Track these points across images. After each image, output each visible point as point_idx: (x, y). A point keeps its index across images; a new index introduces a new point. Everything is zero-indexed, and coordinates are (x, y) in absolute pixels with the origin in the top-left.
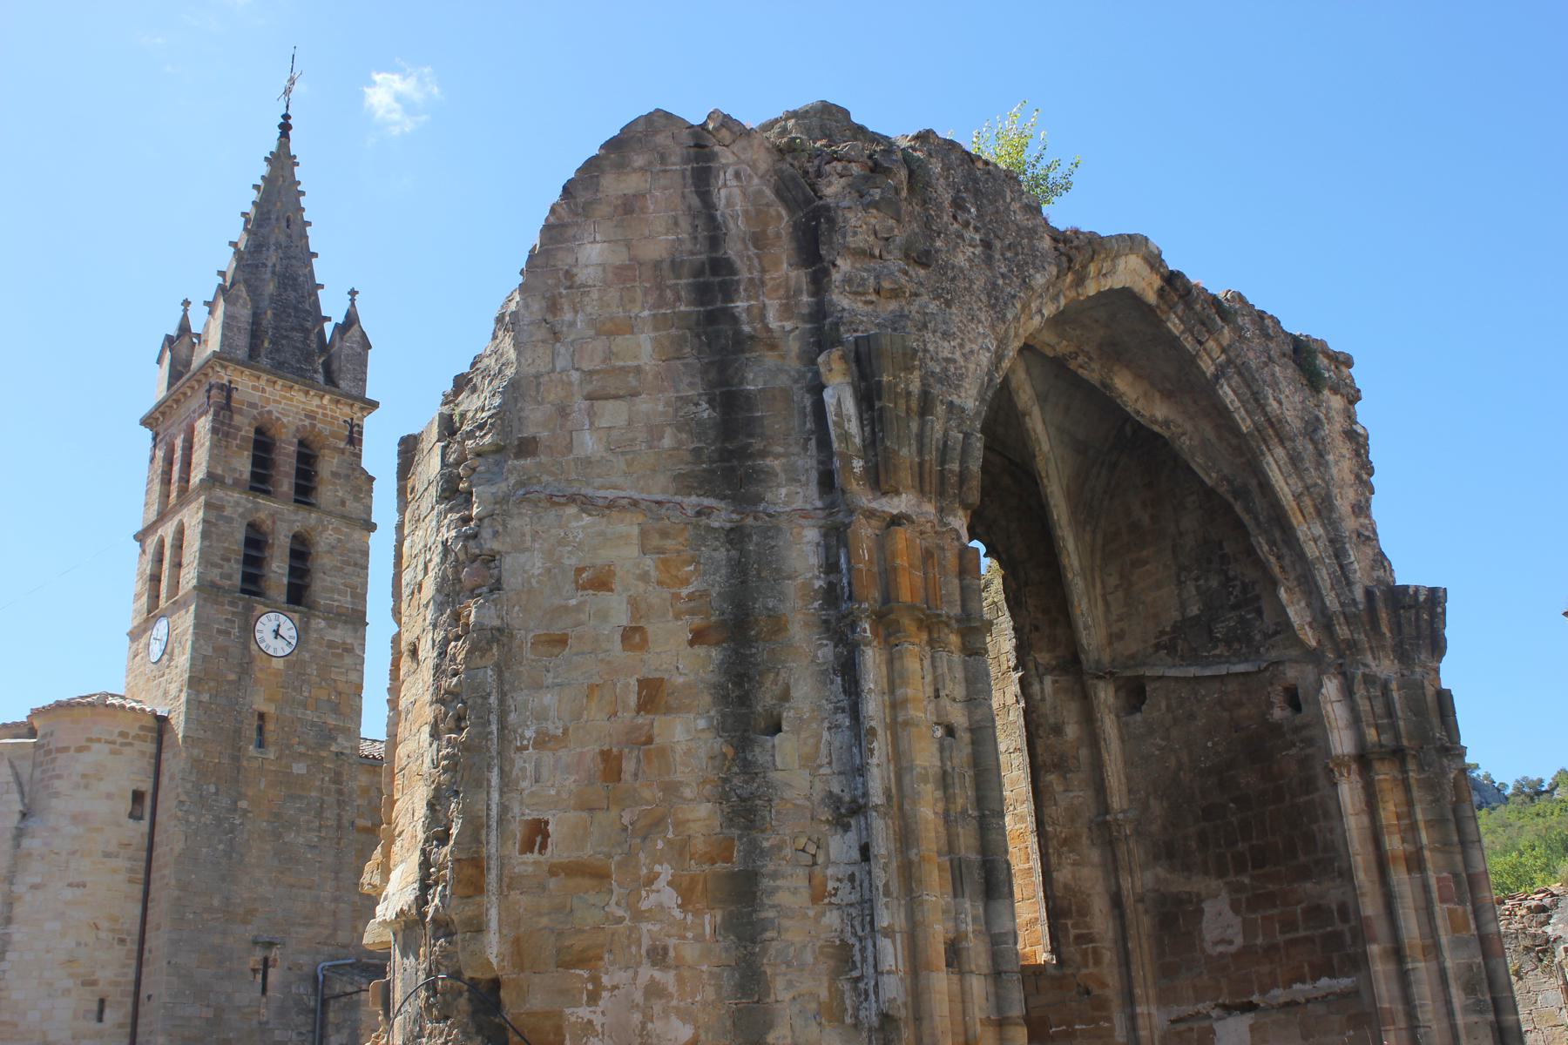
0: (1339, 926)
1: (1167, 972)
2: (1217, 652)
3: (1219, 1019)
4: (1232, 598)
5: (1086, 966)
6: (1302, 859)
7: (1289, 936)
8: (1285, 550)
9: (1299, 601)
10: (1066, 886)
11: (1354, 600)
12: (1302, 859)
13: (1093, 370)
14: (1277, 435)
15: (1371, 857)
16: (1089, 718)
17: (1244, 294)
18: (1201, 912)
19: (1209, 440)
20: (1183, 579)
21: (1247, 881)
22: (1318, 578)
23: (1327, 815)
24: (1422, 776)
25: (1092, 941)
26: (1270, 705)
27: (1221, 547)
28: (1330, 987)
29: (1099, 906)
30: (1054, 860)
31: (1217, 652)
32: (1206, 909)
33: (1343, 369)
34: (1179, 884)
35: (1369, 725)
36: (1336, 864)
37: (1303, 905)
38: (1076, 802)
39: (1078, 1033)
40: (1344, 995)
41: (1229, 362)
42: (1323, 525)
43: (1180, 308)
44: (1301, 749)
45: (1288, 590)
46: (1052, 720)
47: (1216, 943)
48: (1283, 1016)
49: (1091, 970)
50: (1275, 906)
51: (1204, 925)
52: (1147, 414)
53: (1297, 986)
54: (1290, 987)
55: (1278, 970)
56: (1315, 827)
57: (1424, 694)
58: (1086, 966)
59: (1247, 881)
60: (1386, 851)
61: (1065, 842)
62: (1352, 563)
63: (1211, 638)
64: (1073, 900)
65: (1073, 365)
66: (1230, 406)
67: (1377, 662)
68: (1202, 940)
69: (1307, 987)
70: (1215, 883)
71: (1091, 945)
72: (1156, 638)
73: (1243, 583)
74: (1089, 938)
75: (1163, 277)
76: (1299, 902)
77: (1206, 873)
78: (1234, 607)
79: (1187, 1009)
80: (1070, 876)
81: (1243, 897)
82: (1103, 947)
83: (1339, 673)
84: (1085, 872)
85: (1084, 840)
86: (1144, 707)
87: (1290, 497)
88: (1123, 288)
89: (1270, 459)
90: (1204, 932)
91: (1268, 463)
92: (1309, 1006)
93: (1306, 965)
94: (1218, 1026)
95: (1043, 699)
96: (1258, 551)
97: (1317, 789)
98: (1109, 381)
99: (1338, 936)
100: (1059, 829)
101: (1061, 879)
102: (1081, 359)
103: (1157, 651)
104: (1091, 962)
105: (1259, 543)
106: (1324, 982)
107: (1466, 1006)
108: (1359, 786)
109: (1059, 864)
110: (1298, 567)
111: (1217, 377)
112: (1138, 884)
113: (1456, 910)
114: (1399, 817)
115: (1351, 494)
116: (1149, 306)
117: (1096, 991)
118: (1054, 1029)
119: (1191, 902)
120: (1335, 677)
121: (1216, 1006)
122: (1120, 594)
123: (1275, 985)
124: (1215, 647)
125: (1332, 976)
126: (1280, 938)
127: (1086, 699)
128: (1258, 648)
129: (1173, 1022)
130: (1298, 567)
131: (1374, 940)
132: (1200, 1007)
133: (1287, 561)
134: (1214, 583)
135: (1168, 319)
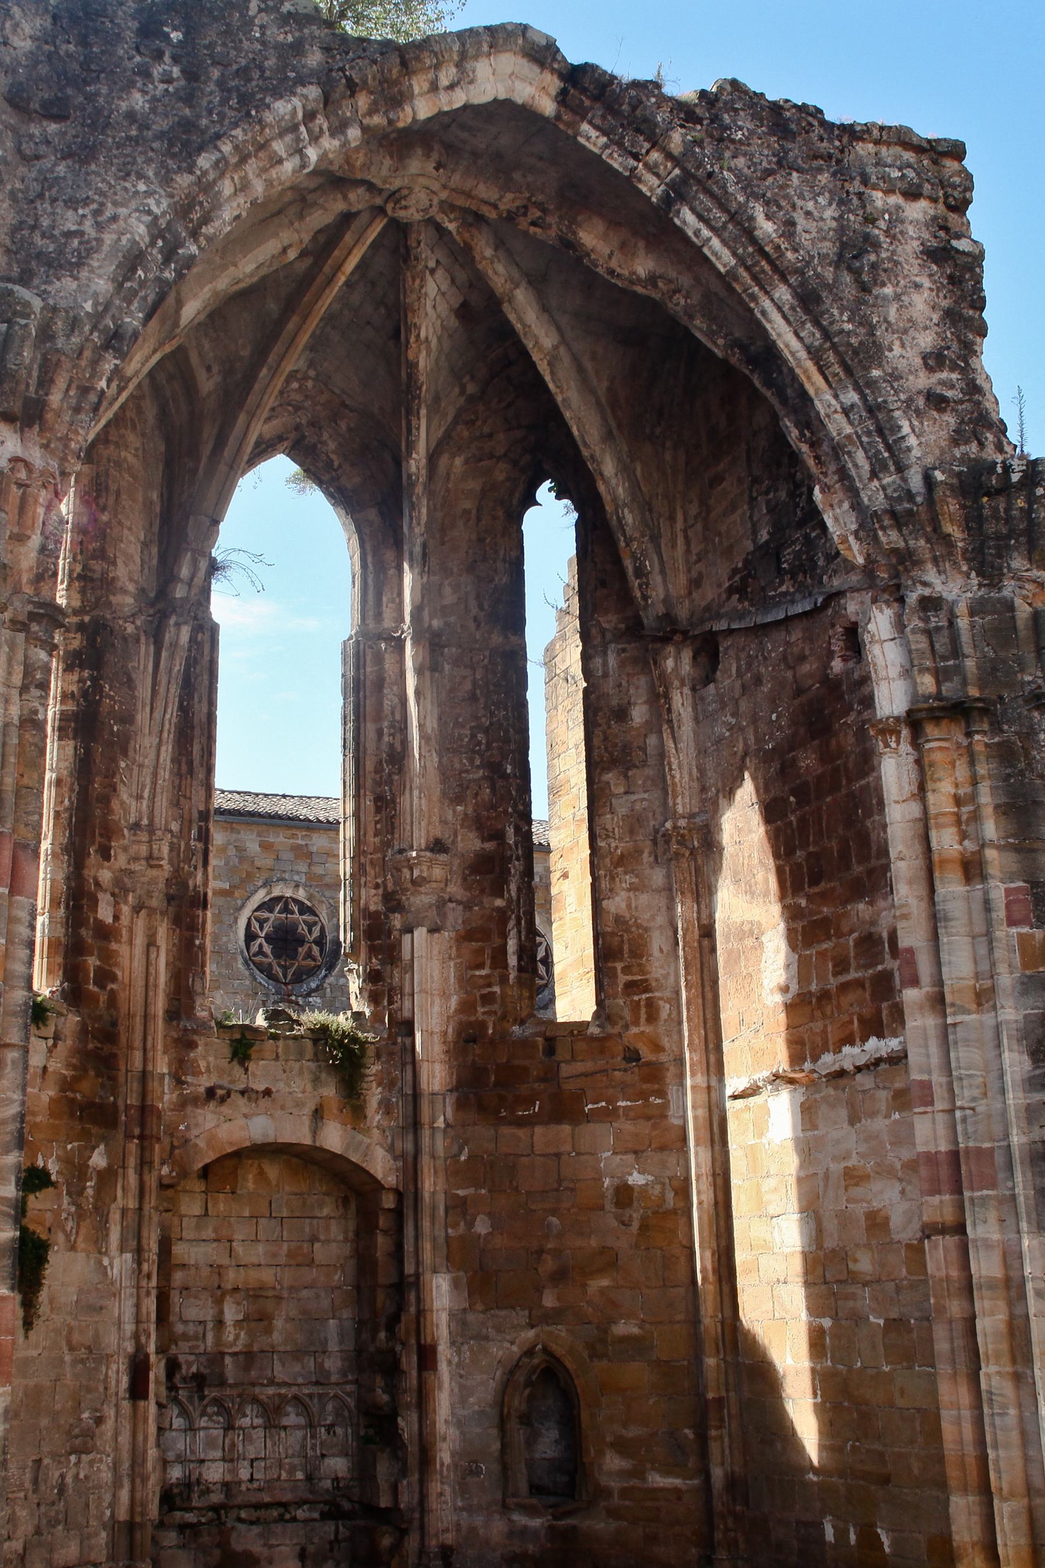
2: (784, 588)
6: (858, 869)
7: (842, 979)
9: (841, 502)
11: (909, 491)
12: (858, 869)
13: (550, 226)
14: (775, 268)
15: (919, 863)
16: (659, 700)
17: (741, 79)
19: (716, 294)
20: (755, 495)
21: (803, 903)
22: (850, 465)
24: (996, 740)
25: (647, 990)
30: (604, 884)
31: (784, 588)
37: (855, 935)
38: (638, 807)
39: (621, 1112)
41: (687, 174)
42: (858, 389)
43: (598, 112)
45: (826, 489)
46: (614, 702)
49: (642, 1029)
53: (847, 1049)
54: (840, 1051)
55: (829, 1029)
57: (1013, 618)
58: (637, 1023)
59: (803, 903)
62: (903, 437)
63: (780, 571)
64: (626, 936)
66: (695, 239)
67: (943, 577)
69: (856, 1050)
71: (644, 996)
72: (729, 579)
75: (562, 76)
76: (851, 932)
80: (623, 905)
82: (661, 998)
84: (644, 899)
85: (646, 858)
87: (803, 354)
88: (495, 100)
89: (767, 304)
91: (764, 313)
92: (858, 1077)
95: (606, 675)
100: (613, 845)
101: (613, 910)
102: (535, 213)
103: (729, 598)
104: (643, 1016)
106: (873, 1042)
107: (1034, 1077)
109: (611, 890)
111: (667, 201)
113: (1032, 936)
114: (958, 801)
116: (546, 120)
117: (647, 1055)
118: (590, 1106)
120: (889, 606)
122: (699, 526)
123: (825, 1049)
125: (880, 1036)
134: (783, 495)
135: (578, 133)
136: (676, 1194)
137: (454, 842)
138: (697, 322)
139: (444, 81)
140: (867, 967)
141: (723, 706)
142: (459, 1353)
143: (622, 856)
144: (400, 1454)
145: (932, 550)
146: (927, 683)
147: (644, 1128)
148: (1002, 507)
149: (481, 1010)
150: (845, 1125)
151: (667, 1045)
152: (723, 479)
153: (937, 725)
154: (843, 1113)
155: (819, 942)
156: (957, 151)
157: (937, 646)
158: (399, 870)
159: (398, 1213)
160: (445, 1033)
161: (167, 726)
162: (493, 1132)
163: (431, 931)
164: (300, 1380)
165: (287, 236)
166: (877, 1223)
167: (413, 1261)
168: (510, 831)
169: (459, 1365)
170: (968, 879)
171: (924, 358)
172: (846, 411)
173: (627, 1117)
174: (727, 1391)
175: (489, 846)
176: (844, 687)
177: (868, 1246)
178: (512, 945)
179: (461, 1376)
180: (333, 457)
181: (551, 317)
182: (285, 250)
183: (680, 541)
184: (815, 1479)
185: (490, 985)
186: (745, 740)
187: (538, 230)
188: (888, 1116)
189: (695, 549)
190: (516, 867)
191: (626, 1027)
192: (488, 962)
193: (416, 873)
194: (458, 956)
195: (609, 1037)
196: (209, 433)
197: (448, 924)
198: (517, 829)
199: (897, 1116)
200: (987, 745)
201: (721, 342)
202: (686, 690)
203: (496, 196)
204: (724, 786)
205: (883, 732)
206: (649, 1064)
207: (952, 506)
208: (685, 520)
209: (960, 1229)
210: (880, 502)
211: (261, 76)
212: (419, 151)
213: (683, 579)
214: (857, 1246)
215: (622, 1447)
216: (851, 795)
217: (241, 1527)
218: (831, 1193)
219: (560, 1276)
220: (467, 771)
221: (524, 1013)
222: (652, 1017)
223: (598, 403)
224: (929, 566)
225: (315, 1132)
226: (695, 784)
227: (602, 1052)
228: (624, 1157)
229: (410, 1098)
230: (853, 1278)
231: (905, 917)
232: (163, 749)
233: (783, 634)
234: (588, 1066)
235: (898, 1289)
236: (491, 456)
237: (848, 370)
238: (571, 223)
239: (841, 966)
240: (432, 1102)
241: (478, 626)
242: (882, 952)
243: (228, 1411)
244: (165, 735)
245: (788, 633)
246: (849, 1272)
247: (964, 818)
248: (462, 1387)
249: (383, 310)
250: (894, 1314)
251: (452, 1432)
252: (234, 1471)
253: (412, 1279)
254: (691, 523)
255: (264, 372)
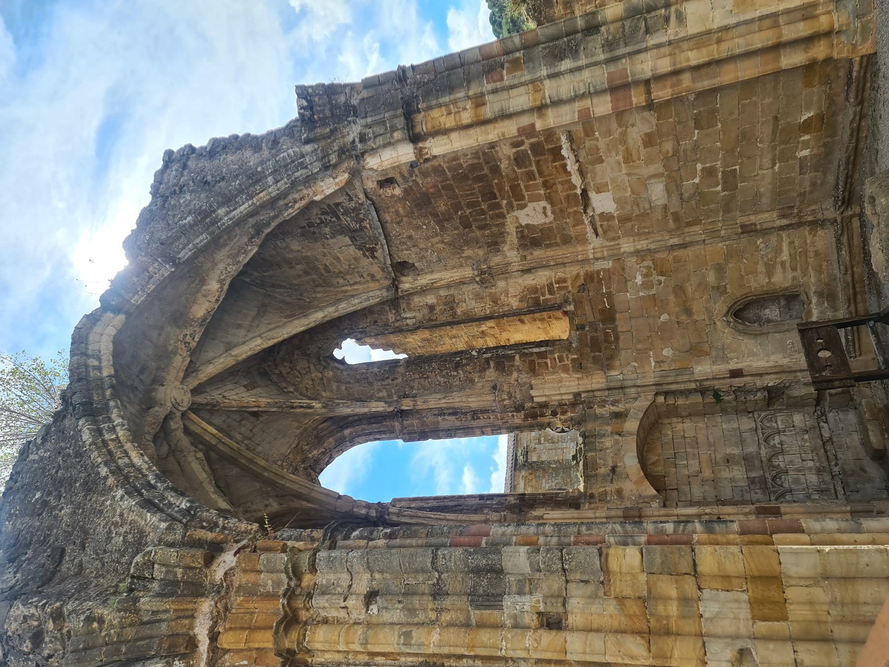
0: (526, 147)
1: (567, 240)
2: (368, 226)
3: (593, 210)
4: (332, 220)
5: (567, 287)
6: (486, 171)
7: (537, 175)
8: (290, 198)
10: (521, 301)
11: (313, 152)
12: (486, 171)
15: (478, 130)
16: (423, 291)
18: (527, 226)
21: (505, 202)
23: (455, 158)
25: (551, 284)
26: (393, 196)
27: (304, 227)
28: (567, 149)
29: (530, 280)
31: (368, 226)
32: (526, 223)
33: (174, 157)
34: (512, 238)
35: (392, 137)
36: (486, 151)
37: (516, 169)
38: (471, 297)
40: (571, 139)
44: (416, 176)
45: (315, 194)
47: (546, 215)
48: (589, 176)
50: (519, 185)
51: (535, 223)
52: (217, 294)
53: (569, 168)
55: (560, 180)
56: (465, 165)
58: (567, 287)
60: (473, 121)
61: (495, 302)
65: (193, 344)
68: (545, 223)
69: (569, 162)
70: (509, 219)
71: (555, 285)
73: (322, 214)
74: (550, 285)
76: (515, 171)
77: (503, 224)
78: (339, 219)
79: (589, 229)
80: (515, 299)
81: (515, 203)
83: (363, 157)
84: (511, 290)
86: (410, 262)
90: (540, 223)
92: (581, 160)
93: (555, 164)
94: (598, 212)
95: (414, 318)
96: (294, 214)
97: (440, 165)
98: (200, 321)
99: (533, 146)
103: (376, 258)
104: (500, 603)
105: (288, 215)
106: (564, 152)
108: (432, 141)
109: (508, 305)
110: (300, 188)
112: (515, 259)
115: (248, 153)
117: (581, 281)
119: (522, 232)
121: (585, 212)
122: (348, 277)
123: (569, 181)
124: (366, 227)
125: (560, 148)
126: (539, 181)
127: (410, 295)
128: (360, 204)
129: (597, 235)
130: (300, 188)
131: (533, 126)
132: (586, 222)
133: (296, 196)
134: (327, 230)
136: (644, 260)
137: (491, 381)
138: (241, 259)
139: (96, 363)
140: (530, 160)
141: (423, 257)
142: (732, 359)
143: (493, 302)
144: (787, 384)
145: (338, 138)
146: (397, 135)
147: (615, 278)
148: (318, 108)
149: (566, 362)
150: (605, 164)
151: (577, 272)
152: (325, 265)
153: (415, 126)
154: (598, 167)
155: (521, 190)
156: (169, 154)
157: (381, 132)
158: (505, 406)
159: (666, 394)
160: (578, 379)
161: (437, 516)
162: (623, 352)
163: (532, 389)
164: (756, 438)
165: (191, 458)
166: (649, 140)
167: (689, 384)
168: (485, 356)
169: (738, 358)
170: (484, 104)
171: (255, 152)
172: (277, 182)
173: (610, 288)
174: (737, 224)
175: (492, 364)
176: (406, 186)
177: (660, 144)
178: (536, 350)
179: (743, 357)
180: (320, 451)
181: (248, 341)
182: (197, 459)
183: (355, 287)
184: (778, 165)
185: (555, 359)
186: (437, 243)
187: (197, 336)
188: (597, 139)
189: (358, 279)
190: (501, 352)
191: (569, 292)
192: (544, 360)
193: (506, 397)
194: (543, 375)
195: (574, 300)
196: (297, 504)
197: (528, 381)
198: (484, 353)
199: (597, 133)
200: (423, 102)
201: (249, 248)
202: (419, 278)
203: (180, 357)
204: (459, 253)
205: (421, 155)
206: (585, 280)
207: (318, 131)
208: (346, 285)
209: (647, 82)
210: (318, 164)
211: (69, 448)
212: (153, 394)
213: (372, 285)
214: (660, 152)
215: (770, 273)
216: (454, 177)
217: (840, 462)
218: (637, 171)
219: (688, 312)
220: (460, 378)
221: (567, 343)
222: (564, 280)
223: (291, 321)
224: (346, 140)
225: (631, 434)
226: (460, 270)
227: (581, 302)
228: (629, 287)
229: (610, 392)
230: (676, 152)
231: (503, 135)
232: (448, 517)
233: (388, 224)
234: (587, 308)
235: (680, 123)
236: (322, 379)
237: (258, 181)
238: (194, 321)
239: (530, 176)
240: (611, 382)
241: (396, 379)
242: (522, 151)
243: (778, 473)
244: (441, 517)
245: (386, 222)
246: (673, 156)
247: (456, 110)
248: (749, 356)
249: (243, 422)
250: (692, 123)
251: (773, 358)
252: (810, 469)
253: (698, 384)
254: (347, 283)
255: (266, 474)
